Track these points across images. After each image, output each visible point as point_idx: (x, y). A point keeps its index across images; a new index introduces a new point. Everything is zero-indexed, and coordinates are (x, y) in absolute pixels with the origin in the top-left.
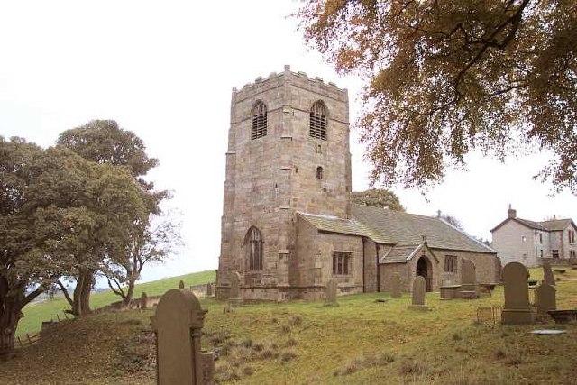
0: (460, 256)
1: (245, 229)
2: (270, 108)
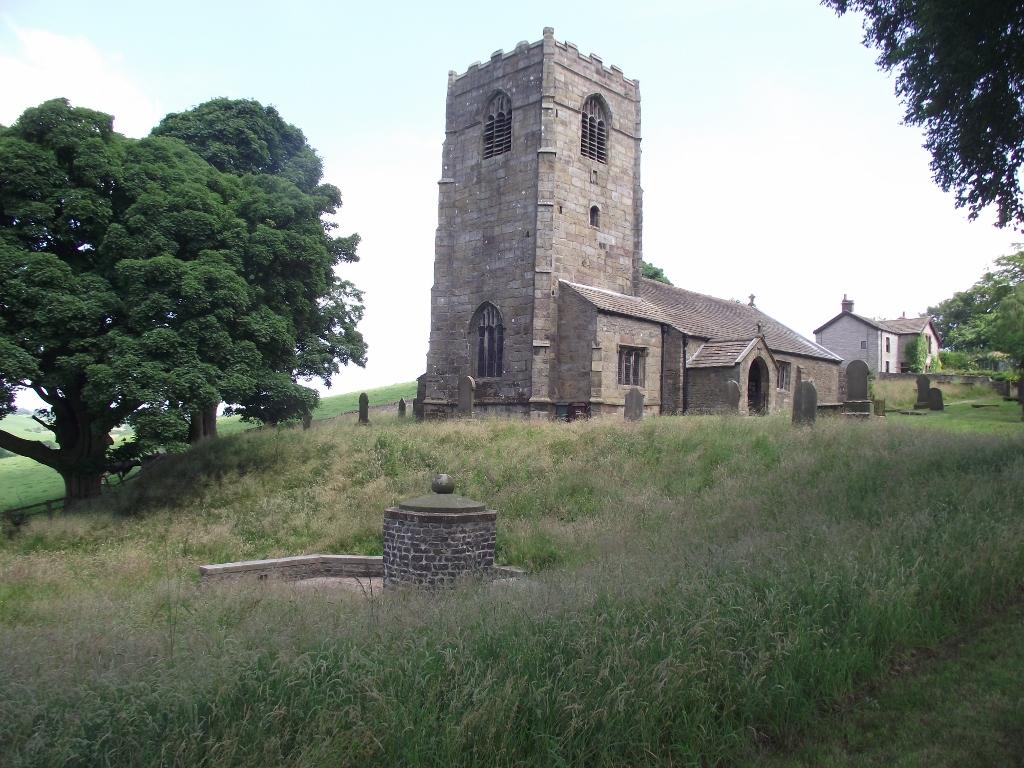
0: (795, 363)
1: (471, 308)
2: (517, 104)
